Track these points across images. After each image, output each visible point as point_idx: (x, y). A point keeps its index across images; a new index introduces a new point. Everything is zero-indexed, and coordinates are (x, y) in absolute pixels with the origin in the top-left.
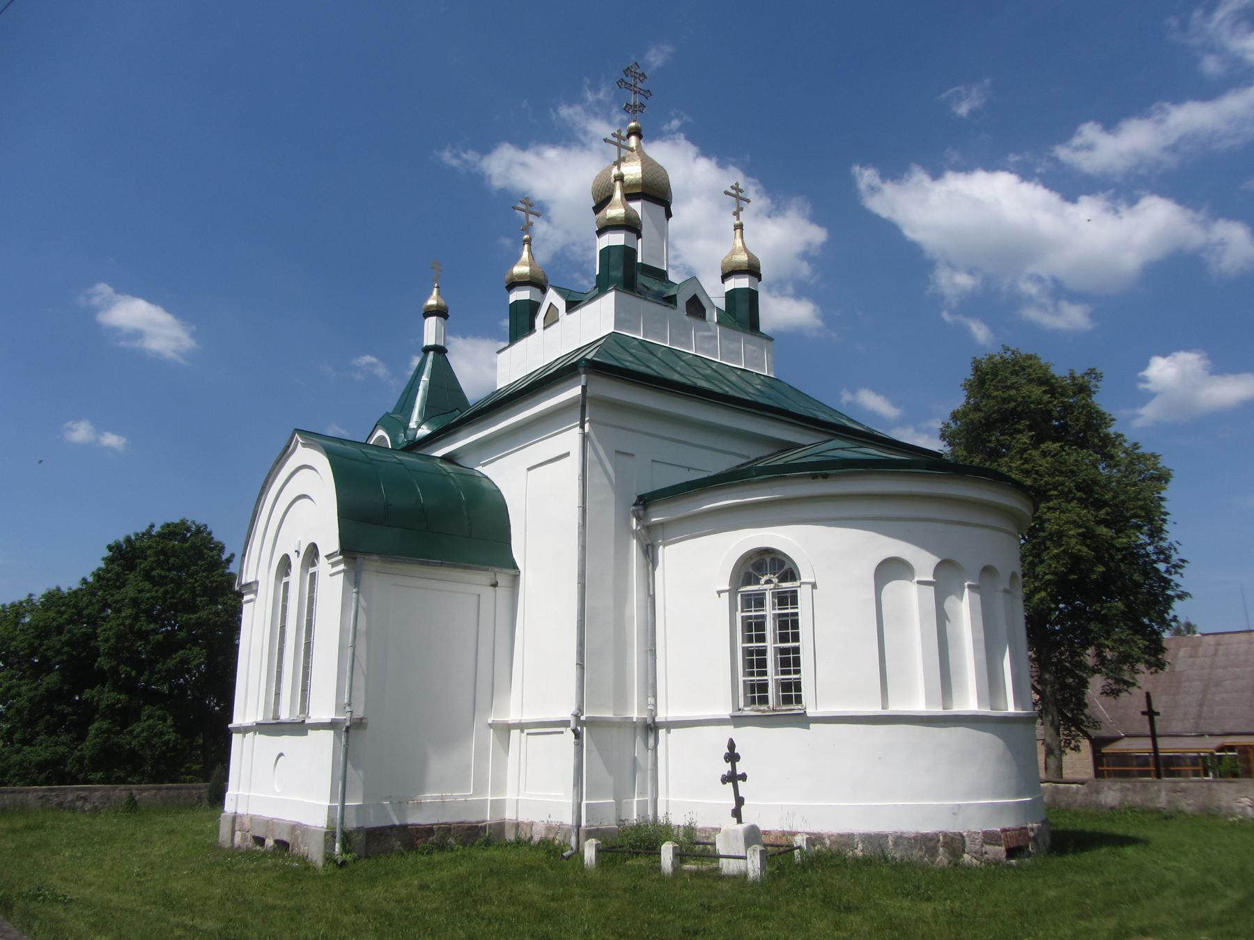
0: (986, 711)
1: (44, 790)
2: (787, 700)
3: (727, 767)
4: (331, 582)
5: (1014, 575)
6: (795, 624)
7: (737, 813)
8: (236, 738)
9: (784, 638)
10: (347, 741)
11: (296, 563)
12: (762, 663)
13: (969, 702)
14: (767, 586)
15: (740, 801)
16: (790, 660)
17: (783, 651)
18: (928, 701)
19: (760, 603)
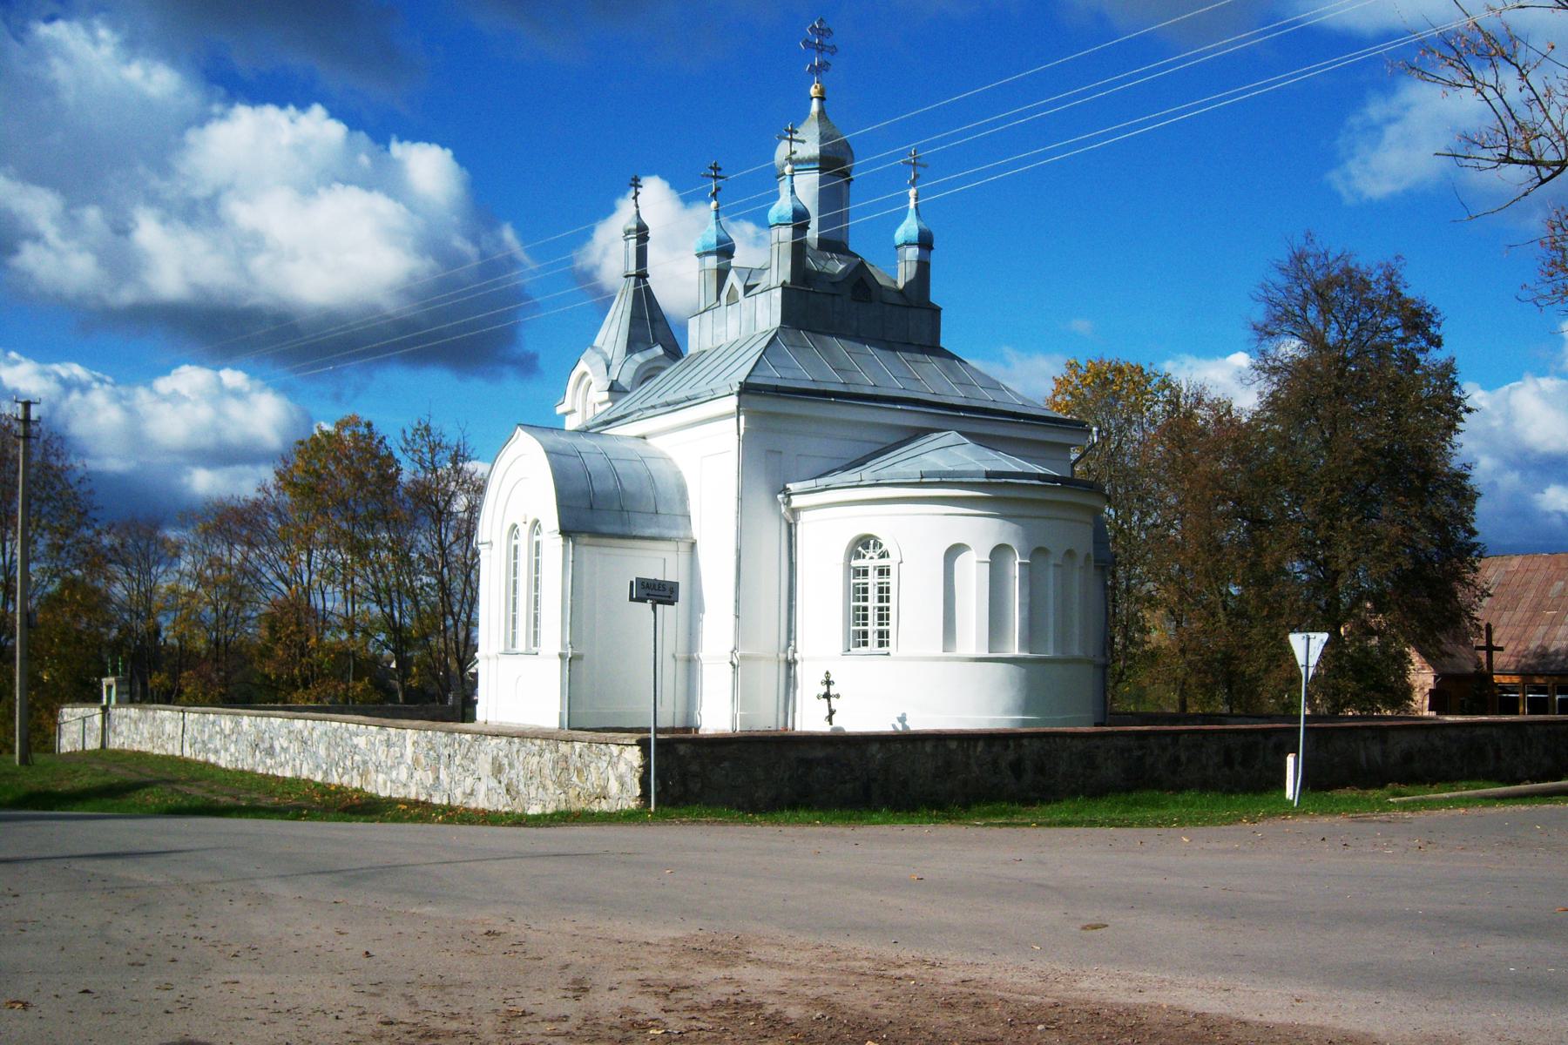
0: (1059, 655)
1: (574, 395)
2: (881, 644)
3: (824, 689)
4: (553, 544)
5: (1088, 556)
6: (888, 590)
7: (830, 719)
8: (115, 743)
9: (881, 600)
10: (1513, 551)
11: (524, 530)
12: (865, 617)
13: (1076, 651)
14: (870, 561)
15: (832, 712)
16: (883, 617)
17: (881, 609)
18: (1021, 648)
19: (865, 573)
